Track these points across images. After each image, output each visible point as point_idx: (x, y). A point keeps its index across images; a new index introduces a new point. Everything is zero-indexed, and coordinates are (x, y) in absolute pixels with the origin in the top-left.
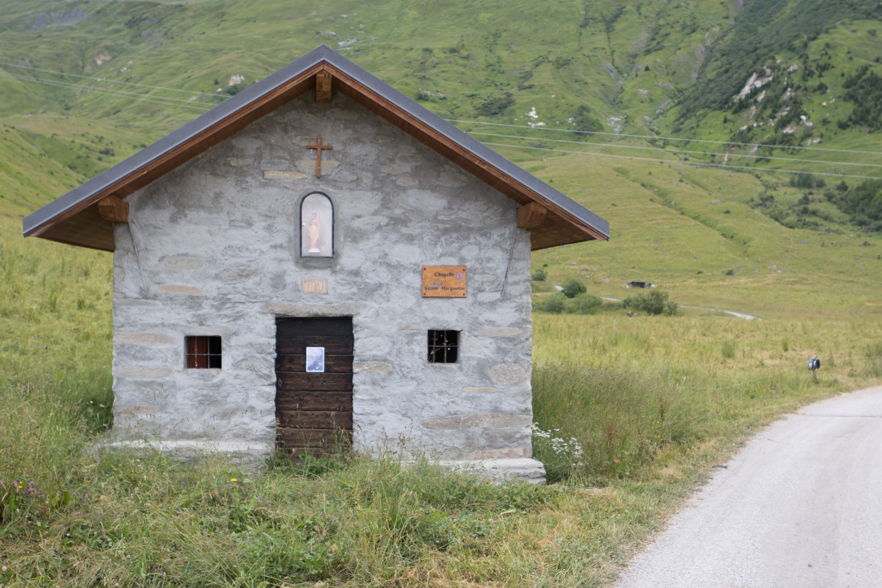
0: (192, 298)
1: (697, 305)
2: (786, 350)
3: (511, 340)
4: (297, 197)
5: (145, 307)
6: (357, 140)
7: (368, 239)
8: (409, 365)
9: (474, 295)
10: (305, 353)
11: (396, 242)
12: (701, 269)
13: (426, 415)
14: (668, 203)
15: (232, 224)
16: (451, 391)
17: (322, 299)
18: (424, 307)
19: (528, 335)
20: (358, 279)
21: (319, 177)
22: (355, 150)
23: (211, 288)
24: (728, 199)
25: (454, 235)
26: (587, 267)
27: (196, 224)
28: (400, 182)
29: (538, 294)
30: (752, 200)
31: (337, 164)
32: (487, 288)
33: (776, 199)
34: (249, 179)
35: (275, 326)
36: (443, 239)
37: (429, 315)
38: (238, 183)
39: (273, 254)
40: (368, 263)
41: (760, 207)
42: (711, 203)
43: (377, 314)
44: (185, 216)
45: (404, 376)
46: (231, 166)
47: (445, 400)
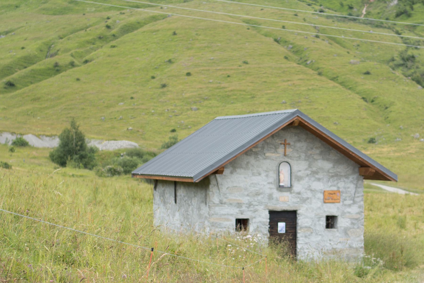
0: (238, 203)
3: (356, 219)
4: (277, 163)
5: (221, 207)
6: (299, 141)
7: (303, 180)
8: (318, 229)
9: (343, 202)
10: (277, 225)
11: (314, 181)
14: (303, 62)
15: (253, 174)
16: (334, 240)
17: (286, 204)
19: (363, 217)
20: (300, 196)
21: (285, 155)
22: (298, 145)
23: (245, 200)
24: (368, 58)
25: (335, 178)
27: (240, 174)
30: (393, 60)
31: (292, 150)
33: (417, 59)
34: (259, 156)
35: (269, 215)
36: (331, 180)
37: (326, 210)
38: (255, 158)
39: (269, 186)
41: (401, 68)
42: (350, 63)
43: (307, 209)
44: (236, 171)
45: (317, 234)
46: (252, 151)
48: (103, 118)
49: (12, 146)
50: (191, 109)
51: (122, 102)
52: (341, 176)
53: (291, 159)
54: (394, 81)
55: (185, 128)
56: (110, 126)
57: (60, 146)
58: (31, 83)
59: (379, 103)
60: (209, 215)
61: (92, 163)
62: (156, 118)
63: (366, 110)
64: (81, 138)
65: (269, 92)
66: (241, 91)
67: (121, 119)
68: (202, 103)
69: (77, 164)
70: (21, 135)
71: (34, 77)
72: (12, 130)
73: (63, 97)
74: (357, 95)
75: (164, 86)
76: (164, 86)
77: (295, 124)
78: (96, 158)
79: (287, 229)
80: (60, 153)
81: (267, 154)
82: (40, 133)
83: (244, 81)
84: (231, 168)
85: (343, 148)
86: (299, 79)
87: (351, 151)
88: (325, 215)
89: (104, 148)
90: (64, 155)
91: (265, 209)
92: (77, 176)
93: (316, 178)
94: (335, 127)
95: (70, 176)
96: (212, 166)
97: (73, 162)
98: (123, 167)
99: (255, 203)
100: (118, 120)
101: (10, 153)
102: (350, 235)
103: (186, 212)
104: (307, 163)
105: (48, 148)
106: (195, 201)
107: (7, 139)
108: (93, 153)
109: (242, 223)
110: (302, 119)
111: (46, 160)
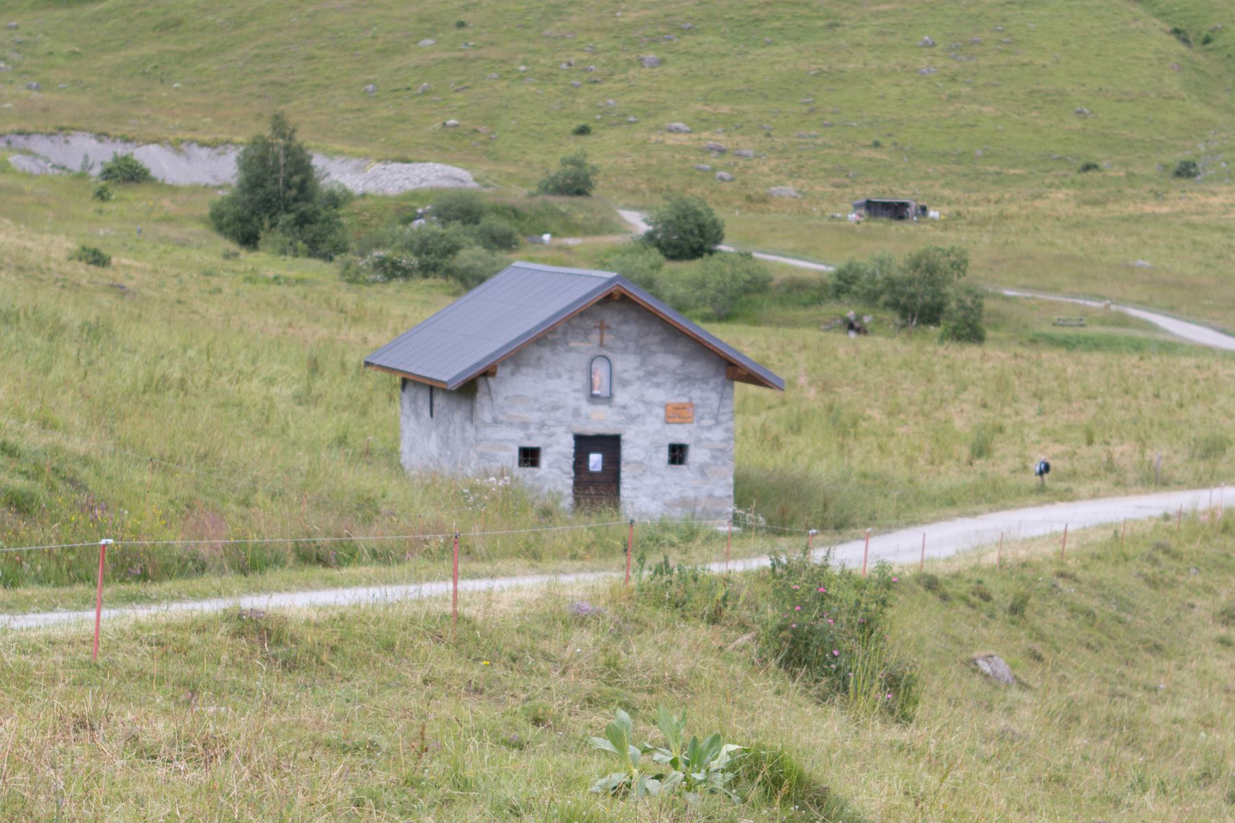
1: (1056, 289)
2: (1090, 442)
3: (721, 450)
4: (587, 358)
6: (626, 322)
12: (1097, 155)
13: (667, 498)
15: (549, 376)
21: (602, 345)
22: (625, 328)
23: (535, 417)
26: (722, 140)
29: (571, 241)
43: (637, 433)
45: (653, 473)
47: (679, 489)
48: (370, 87)
49: (103, 183)
51: (429, 36)
52: (697, 379)
55: (619, 124)
59: (1226, 46)
61: (332, 237)
63: (1180, 69)
64: (300, 165)
65: (883, 8)
67: (426, 92)
69: (288, 239)
74: (1159, 23)
78: (344, 220)
81: (572, 344)
82: (180, 136)
84: (512, 367)
89: (371, 187)
90: (253, 213)
92: (288, 281)
97: (279, 236)
98: (417, 254)
99: (550, 423)
101: (98, 205)
105: (206, 186)
106: (458, 416)
109: (530, 456)
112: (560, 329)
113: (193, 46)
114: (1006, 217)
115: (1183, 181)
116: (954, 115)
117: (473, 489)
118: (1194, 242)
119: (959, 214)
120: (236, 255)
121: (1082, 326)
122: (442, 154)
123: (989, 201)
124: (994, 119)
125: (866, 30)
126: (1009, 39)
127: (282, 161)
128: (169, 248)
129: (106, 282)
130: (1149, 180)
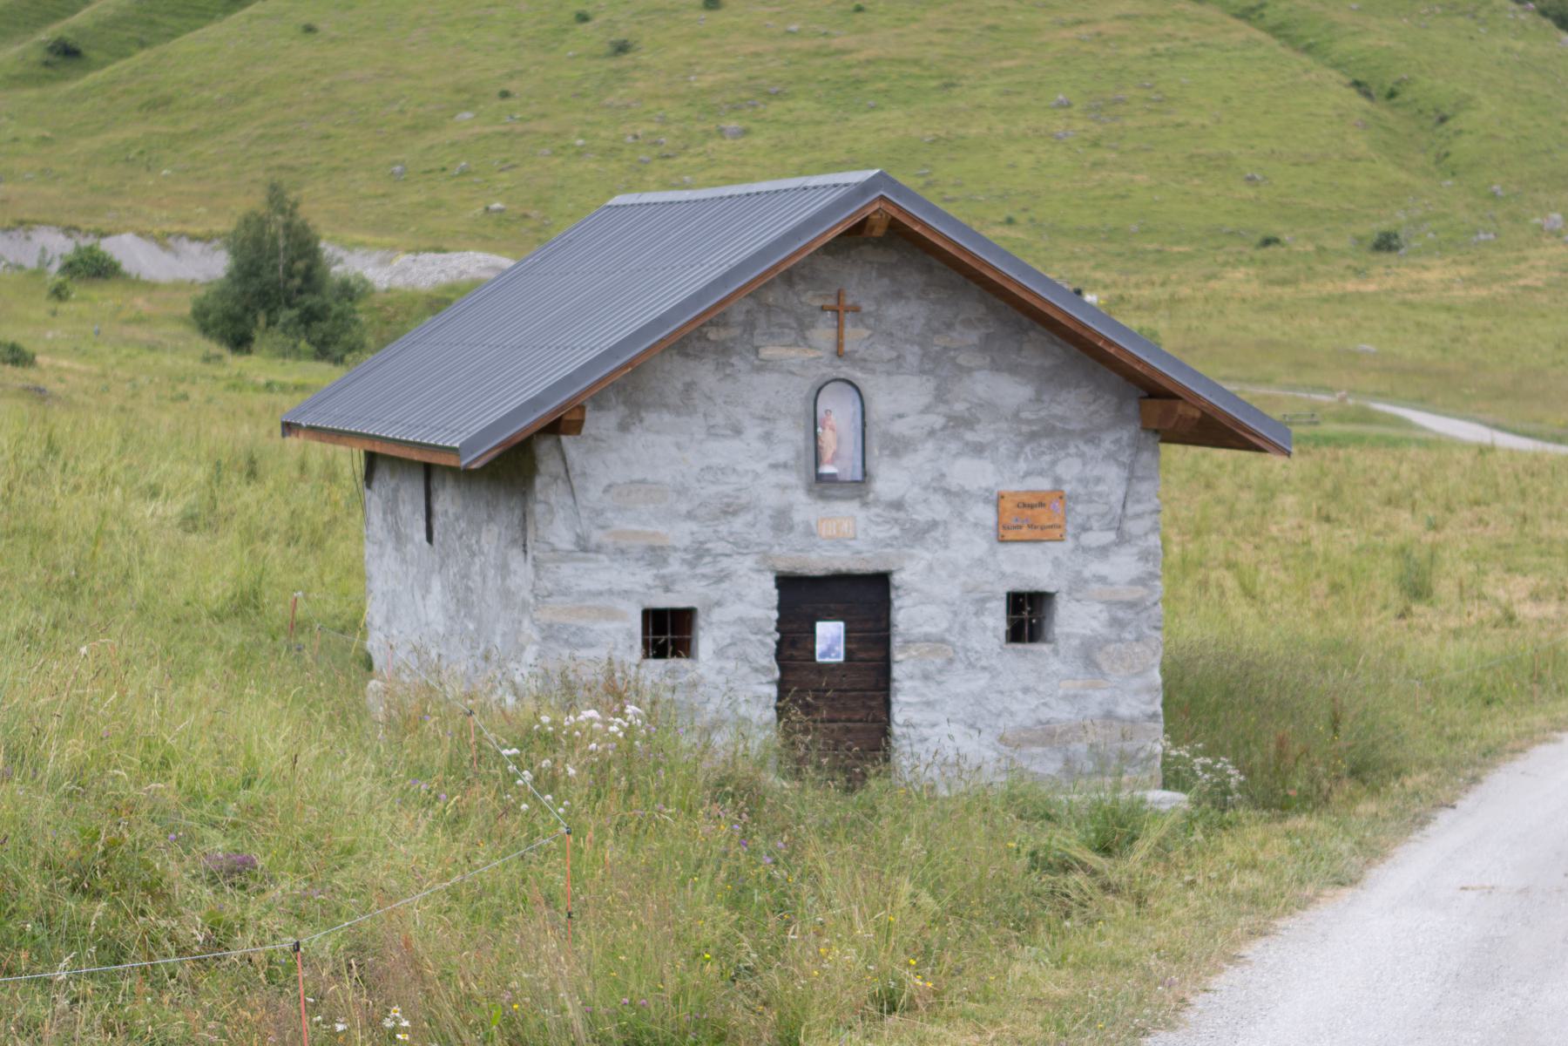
0: (653, 549)
1: (1267, 380)
3: (1131, 605)
4: (807, 386)
5: (583, 565)
6: (897, 295)
7: (915, 451)
8: (979, 648)
9: (1076, 537)
10: (813, 632)
11: (958, 455)
12: (1276, 228)
15: (712, 432)
16: (1041, 688)
17: (847, 546)
18: (1001, 556)
19: (1157, 597)
20: (902, 515)
21: (839, 353)
22: (894, 311)
23: (681, 533)
25: (1045, 442)
27: (658, 432)
28: (962, 359)
32: (1095, 525)
34: (734, 360)
35: (776, 592)
36: (1027, 449)
37: (1008, 568)
38: (719, 367)
40: (916, 490)
43: (930, 568)
44: (641, 421)
45: (971, 665)
47: (1033, 701)
48: (398, 168)
49: (61, 279)
50: (721, 132)
51: (467, 109)
52: (1069, 433)
53: (862, 369)
54: (1474, 17)
56: (423, 198)
57: (230, 275)
58: (142, 45)
59: (1416, 101)
60: (536, 596)
61: (346, 337)
62: (592, 166)
63: (1366, 126)
64: (304, 246)
65: (1006, 64)
66: (902, 62)
67: (464, 173)
68: (762, 107)
69: (291, 341)
70: (103, 235)
71: (152, 23)
72: (67, 220)
73: (257, 93)
74: (1334, 74)
75: (622, 48)
76: (622, 48)
77: (872, 229)
78: (363, 318)
79: (854, 646)
80: (229, 303)
82: (167, 228)
83: (915, 26)
84: (622, 410)
85: (1070, 325)
86: (1118, 18)
87: (1101, 337)
88: (1003, 589)
89: (399, 282)
90: (246, 309)
91: (759, 571)
92: (284, 388)
93: (967, 444)
94: (1251, 192)
95: (257, 389)
96: (534, 403)
99: (719, 547)
100: (453, 177)
101: (53, 304)
102: (1106, 667)
103: (463, 577)
104: (931, 384)
106: (492, 538)
107: (43, 251)
108: (351, 299)
109: (668, 631)
110: (900, 209)
111: (181, 329)
112: (738, 316)
113: (185, 127)
114: (1180, 301)
115: (1384, 256)
116: (1100, 185)
117: (535, 740)
118: (1418, 324)
119: (1122, 298)
120: (219, 357)
121: (1316, 423)
122: (485, 242)
123: (1153, 284)
124: (1149, 188)
125: (988, 91)
126: (1159, 96)
127: (282, 243)
128: (135, 352)
129: (20, 384)
130: (1343, 255)
